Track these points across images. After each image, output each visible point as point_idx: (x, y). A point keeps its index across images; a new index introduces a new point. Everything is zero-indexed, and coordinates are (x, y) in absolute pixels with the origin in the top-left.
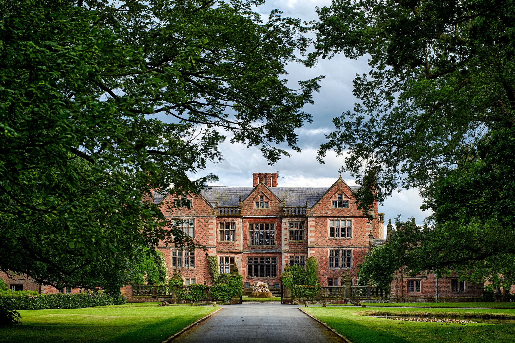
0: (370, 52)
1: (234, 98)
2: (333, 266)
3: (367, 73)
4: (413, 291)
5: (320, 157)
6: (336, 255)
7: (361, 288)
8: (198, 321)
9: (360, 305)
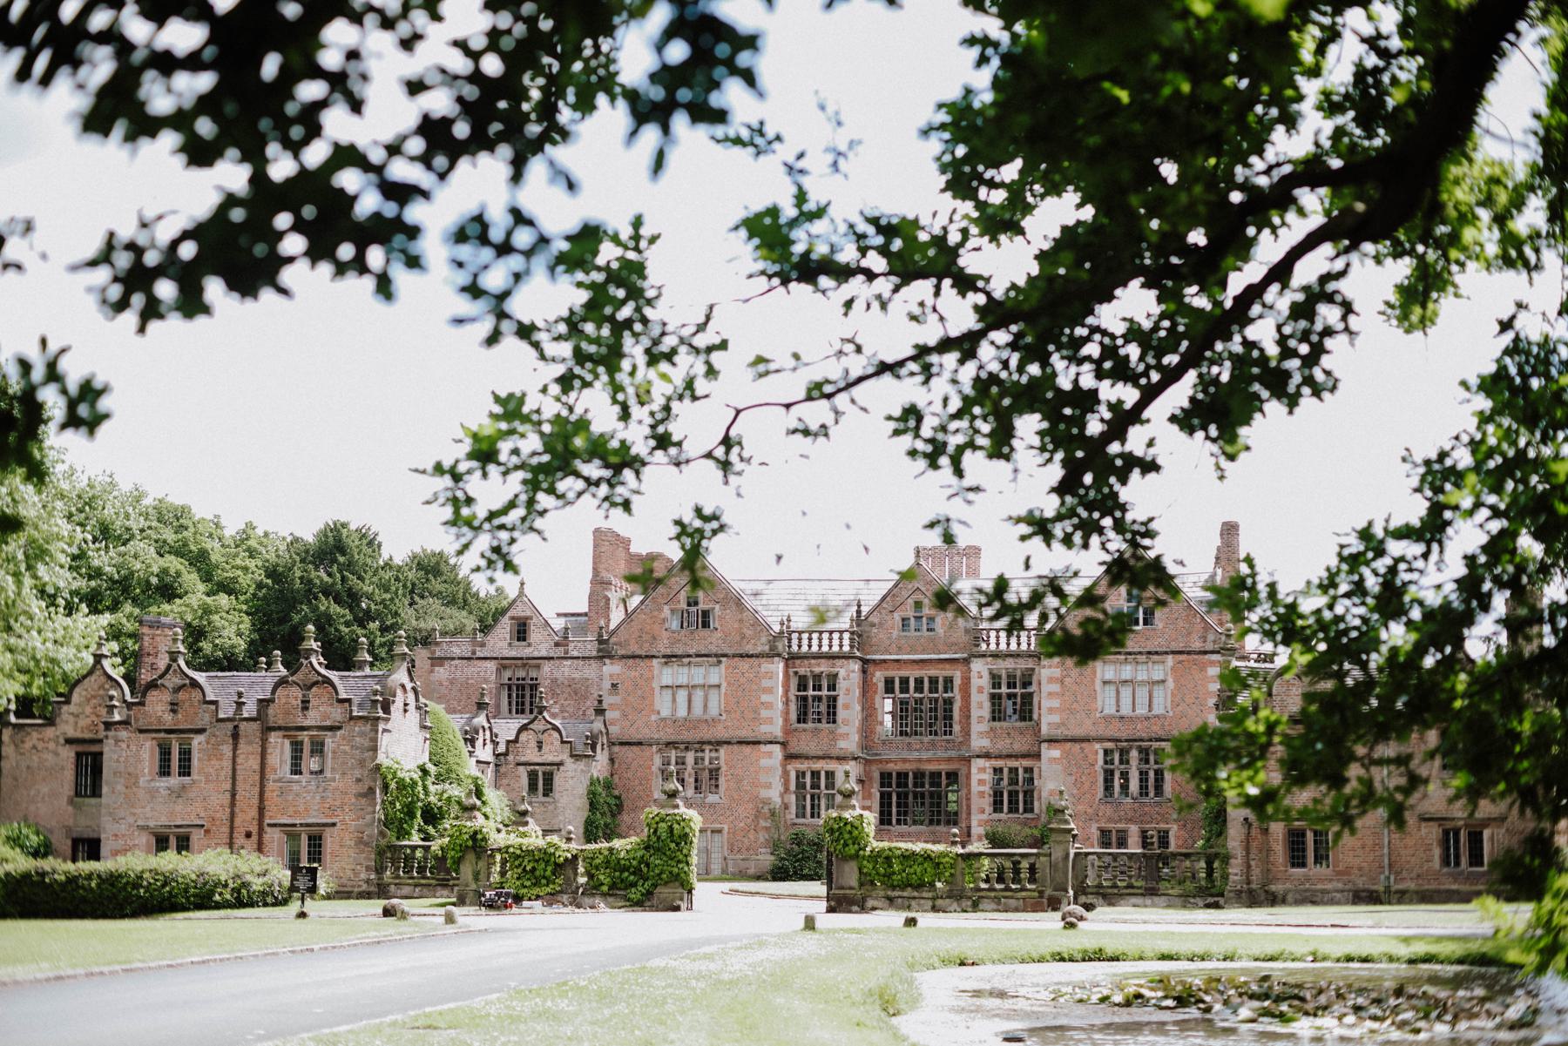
4: (1303, 865)
6: (1121, 762)
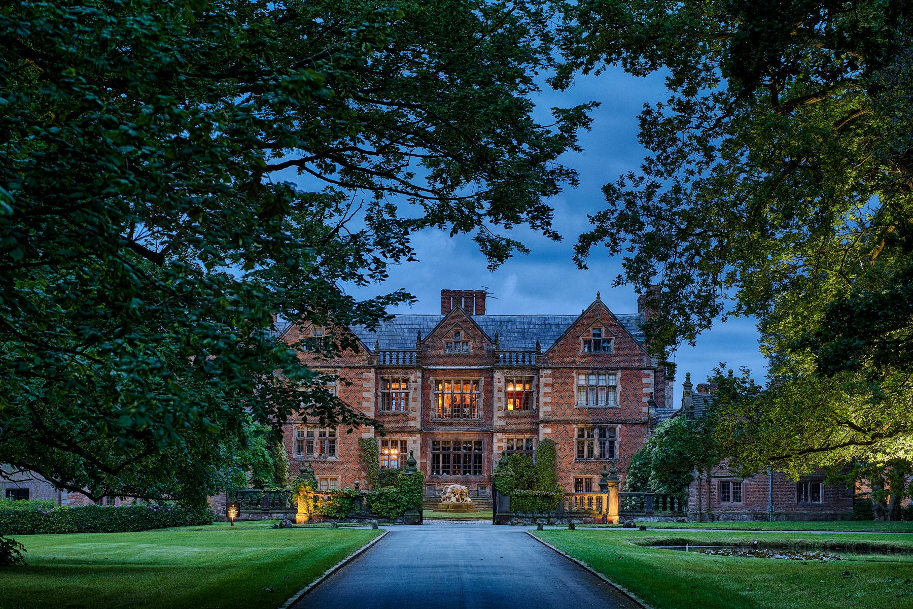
0: (669, 65)
1: (428, 142)
2: (583, 457)
3: (665, 103)
4: (728, 501)
5: (580, 257)
6: (589, 436)
7: (635, 495)
8: (350, 557)
9: (635, 527)
